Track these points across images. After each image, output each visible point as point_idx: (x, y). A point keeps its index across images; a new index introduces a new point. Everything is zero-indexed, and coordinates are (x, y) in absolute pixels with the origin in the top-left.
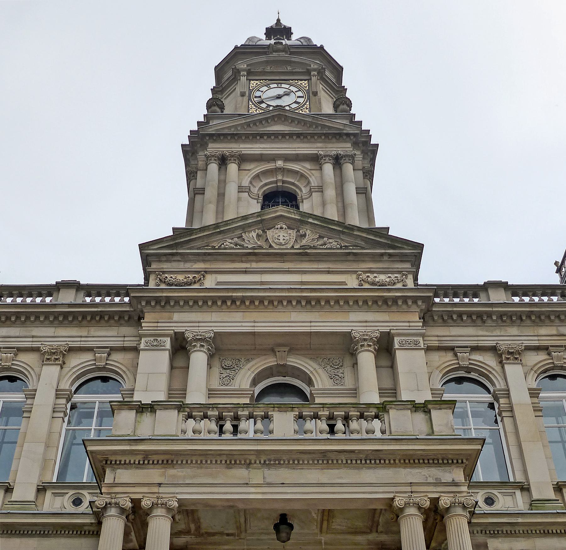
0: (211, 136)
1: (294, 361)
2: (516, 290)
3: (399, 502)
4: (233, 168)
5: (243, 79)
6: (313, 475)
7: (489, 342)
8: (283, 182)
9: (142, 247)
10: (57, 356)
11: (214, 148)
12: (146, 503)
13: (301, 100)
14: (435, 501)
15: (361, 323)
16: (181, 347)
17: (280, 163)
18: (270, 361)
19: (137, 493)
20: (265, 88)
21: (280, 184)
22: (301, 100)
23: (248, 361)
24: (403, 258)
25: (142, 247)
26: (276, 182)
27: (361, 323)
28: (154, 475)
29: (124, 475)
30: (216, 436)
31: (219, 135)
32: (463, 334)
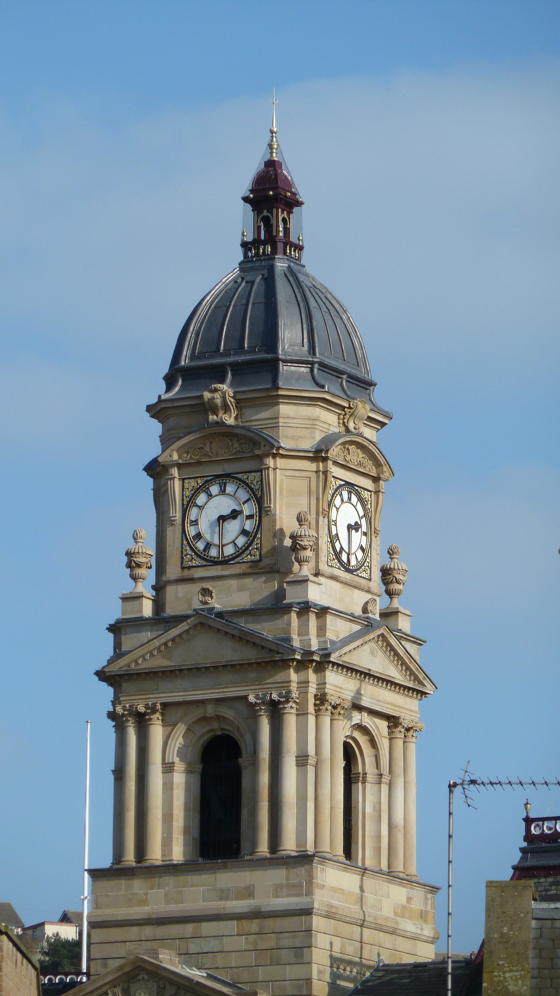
17: (210, 710)
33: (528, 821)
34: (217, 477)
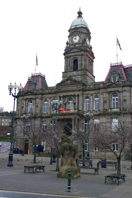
17: (75, 56)
33: (111, 64)
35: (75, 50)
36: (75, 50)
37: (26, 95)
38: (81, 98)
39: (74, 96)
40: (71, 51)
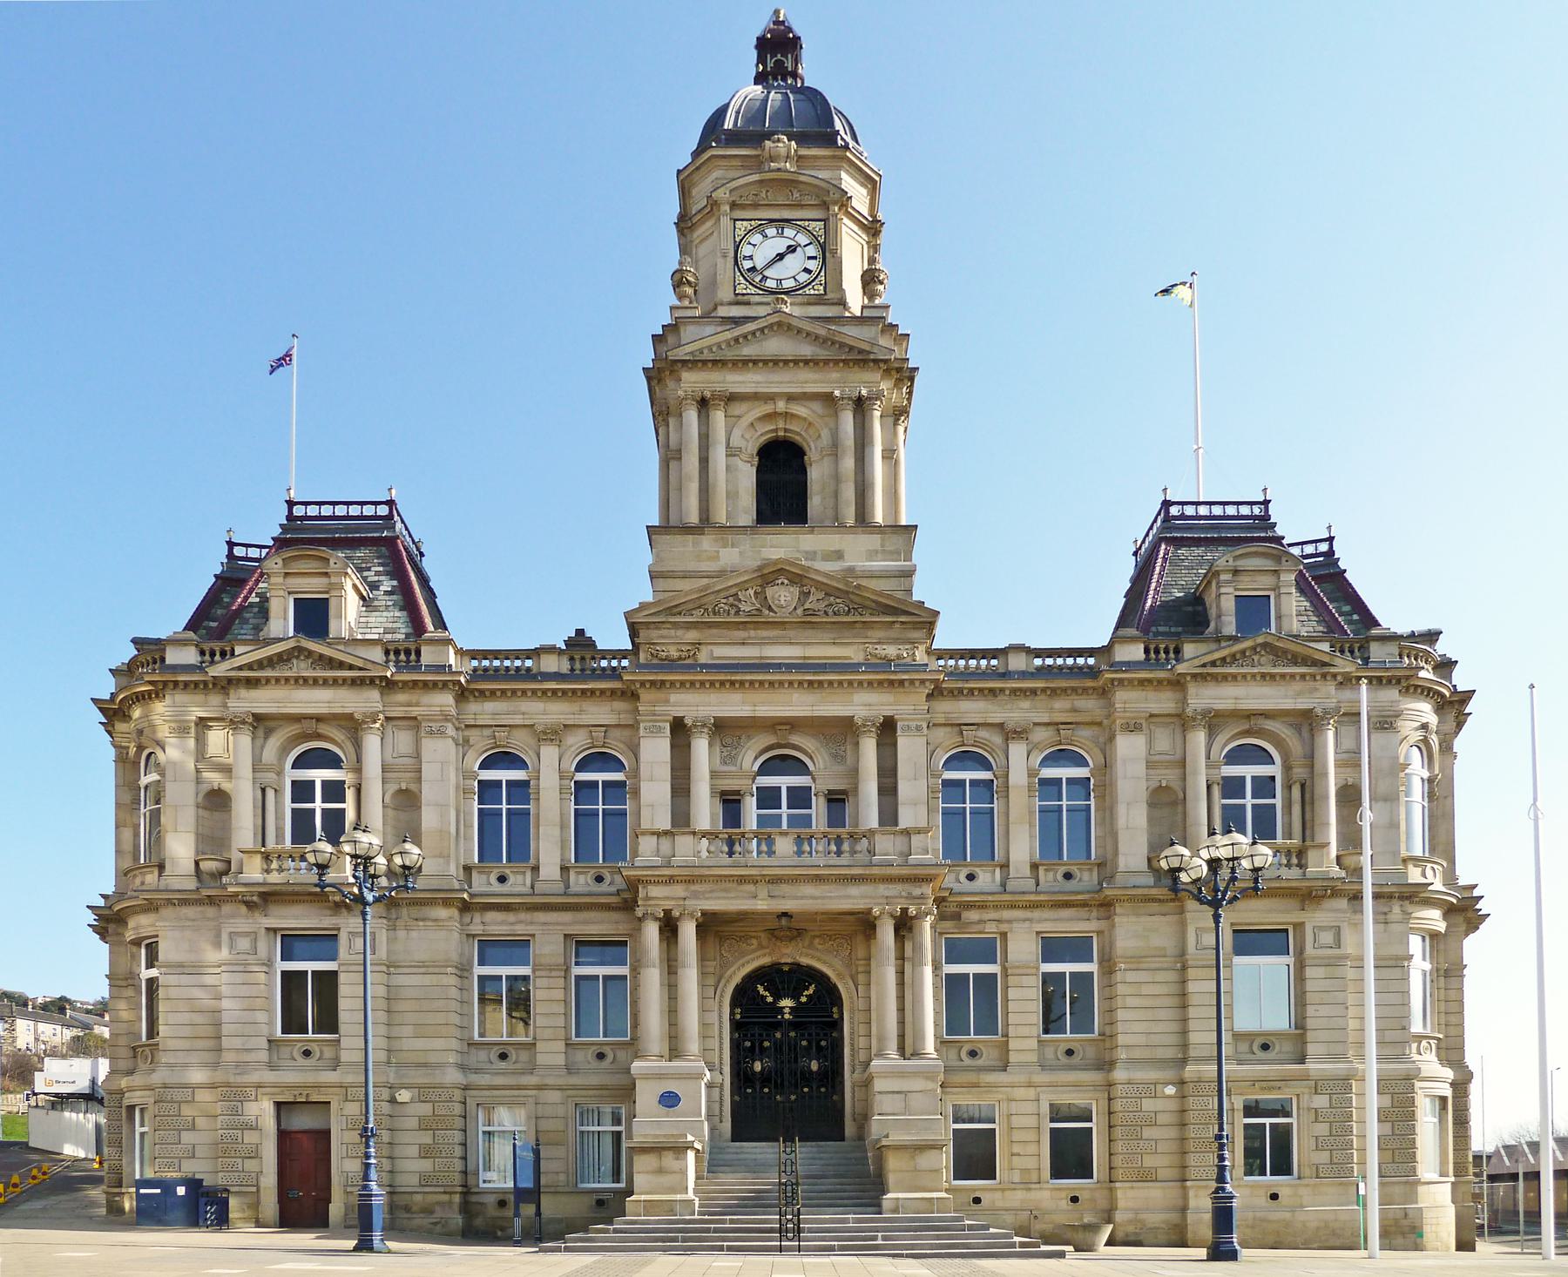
0: (684, 362)
1: (796, 739)
2: (1039, 653)
3: (876, 911)
4: (718, 417)
5: (725, 222)
6: (809, 890)
7: (996, 718)
8: (786, 430)
9: (627, 615)
10: (553, 734)
11: (692, 382)
12: (676, 913)
13: (812, 265)
14: (905, 911)
15: (864, 705)
16: (680, 731)
17: (781, 406)
18: (772, 740)
19: (668, 904)
20: (757, 238)
21: (781, 433)
22: (812, 265)
23: (749, 738)
24: (917, 626)
25: (627, 615)
26: (776, 430)
27: (864, 705)
28: (679, 890)
29: (655, 891)
30: (727, 860)
31: (695, 362)
32: (971, 710)
34: (771, 221)
35: (775, 346)
36: (775, 346)
37: (252, 683)
38: (909, 748)
39: (842, 731)
40: (748, 351)
